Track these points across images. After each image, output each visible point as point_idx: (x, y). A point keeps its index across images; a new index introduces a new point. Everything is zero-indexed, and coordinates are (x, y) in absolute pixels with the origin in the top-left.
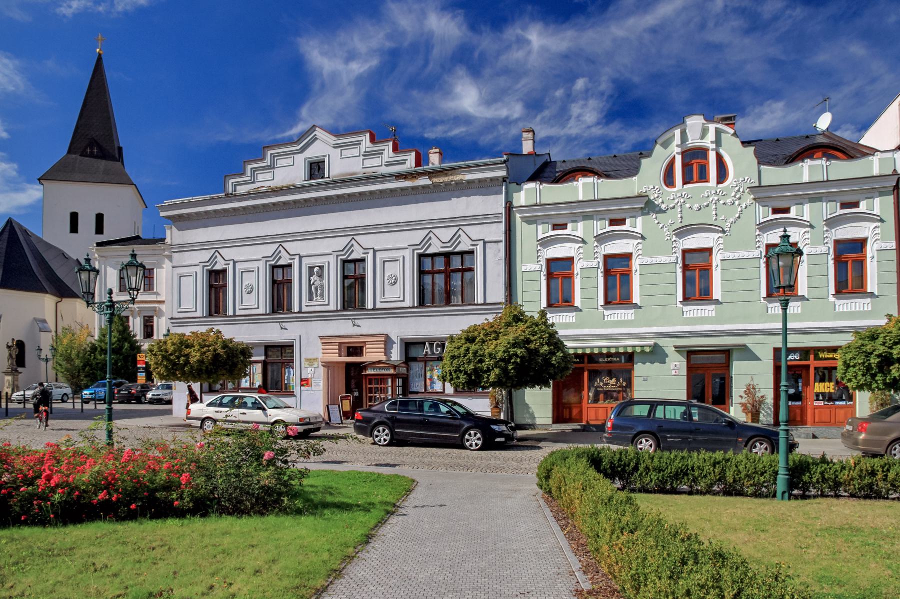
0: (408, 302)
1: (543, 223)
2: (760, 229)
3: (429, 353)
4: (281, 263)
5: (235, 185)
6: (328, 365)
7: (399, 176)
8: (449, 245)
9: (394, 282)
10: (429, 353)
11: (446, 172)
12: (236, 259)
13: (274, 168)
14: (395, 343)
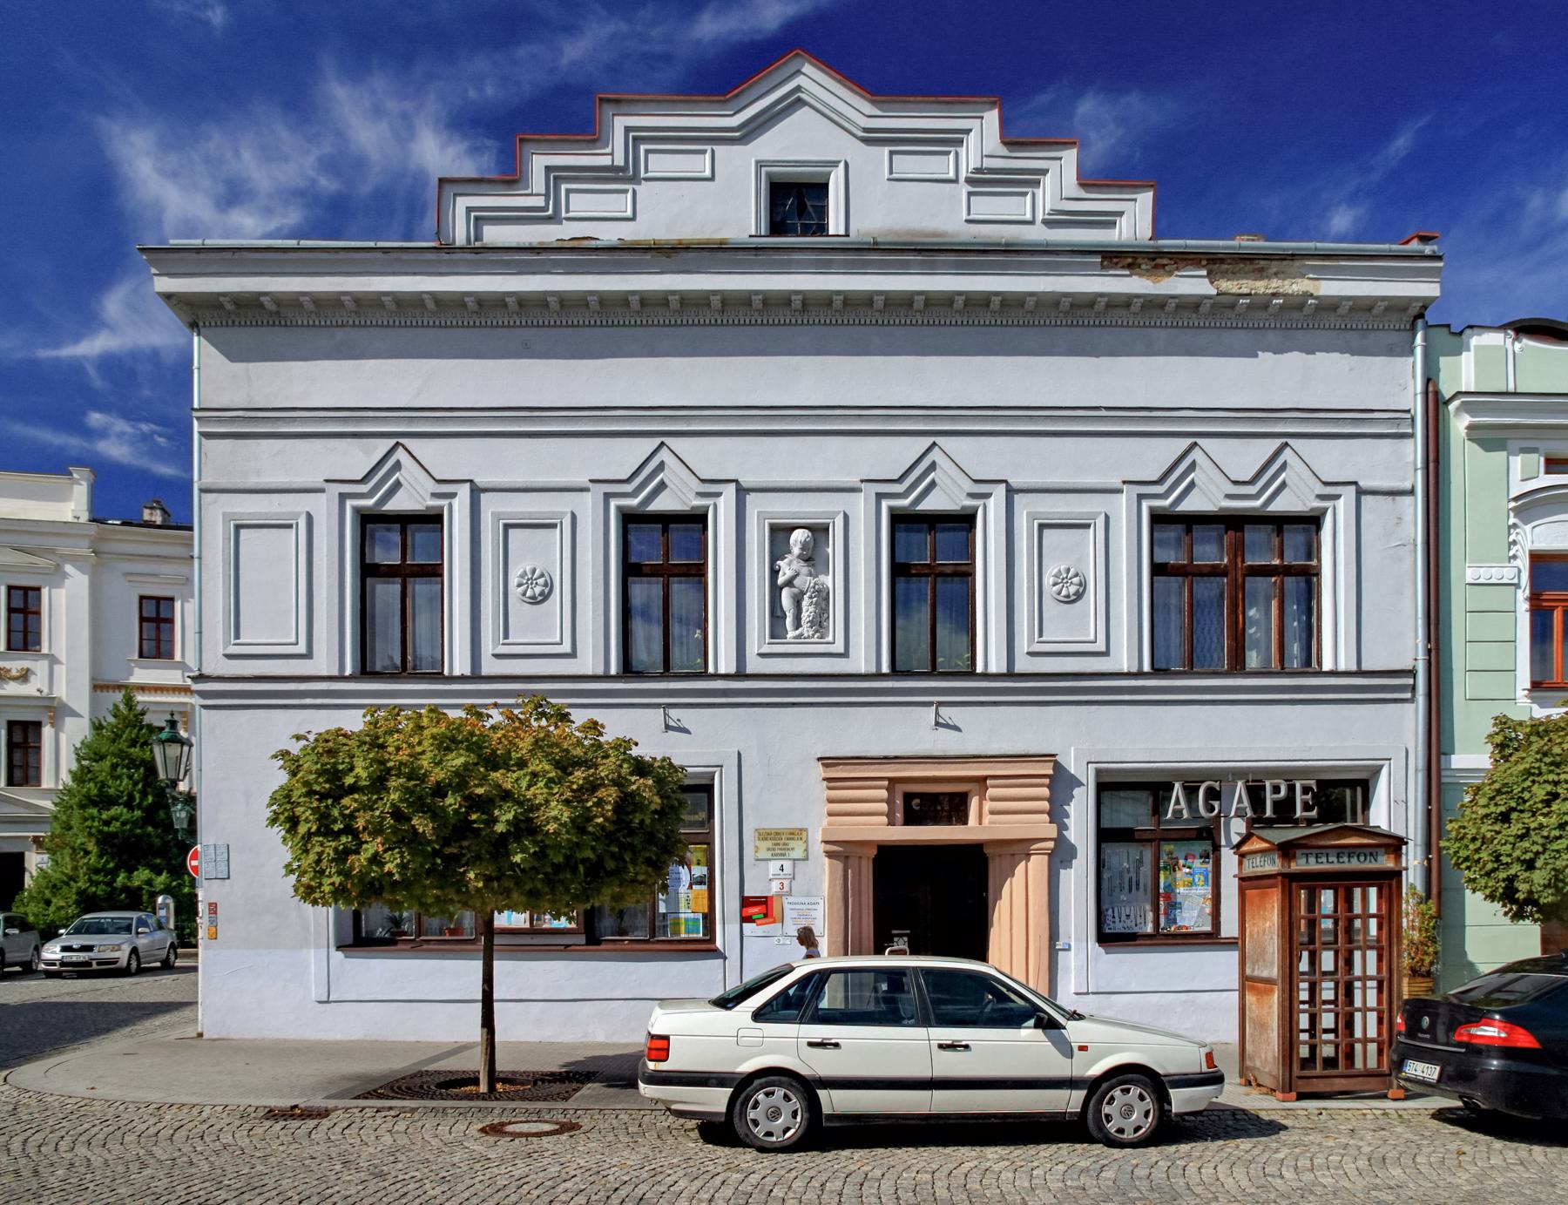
0: (324, 660)
1: (1525, 450)
2: (1518, 511)
3: (1186, 815)
4: (398, 504)
5: (479, 220)
6: (842, 852)
7: (1116, 258)
8: (1252, 490)
9: (542, 593)
10: (1186, 815)
11: (1262, 263)
12: (480, 480)
13: (635, 179)
14: (1080, 784)
